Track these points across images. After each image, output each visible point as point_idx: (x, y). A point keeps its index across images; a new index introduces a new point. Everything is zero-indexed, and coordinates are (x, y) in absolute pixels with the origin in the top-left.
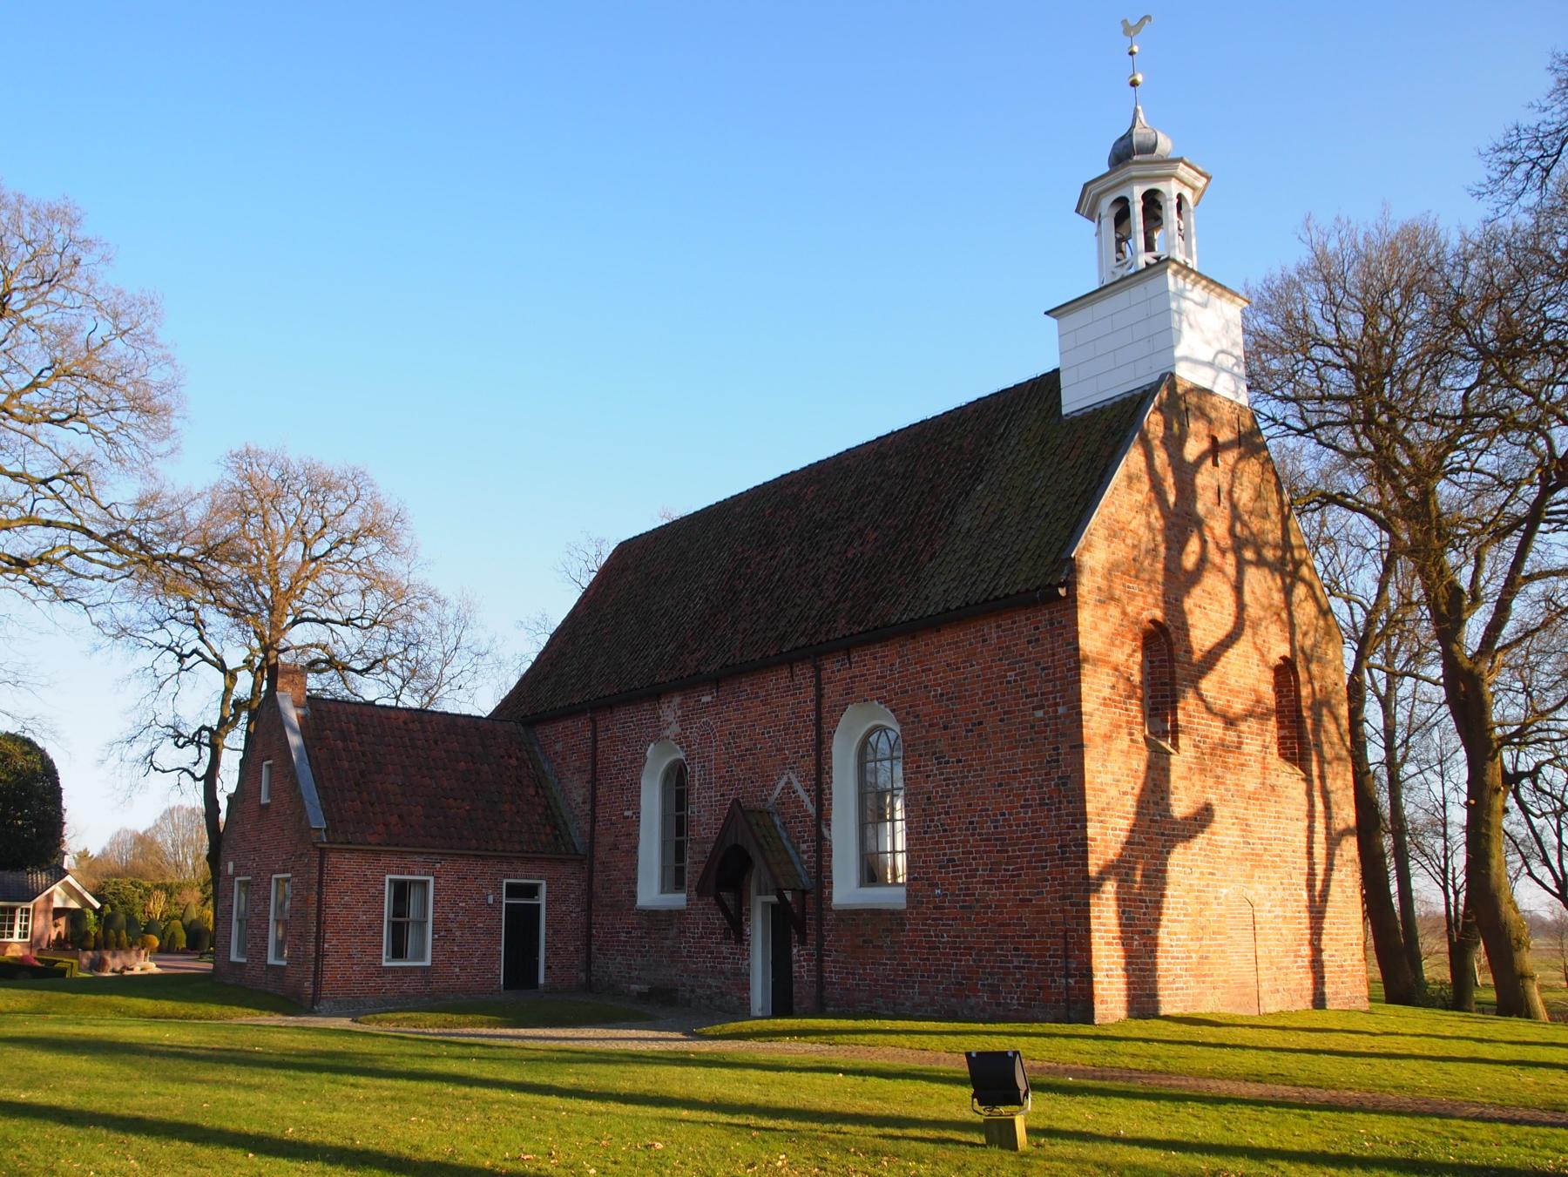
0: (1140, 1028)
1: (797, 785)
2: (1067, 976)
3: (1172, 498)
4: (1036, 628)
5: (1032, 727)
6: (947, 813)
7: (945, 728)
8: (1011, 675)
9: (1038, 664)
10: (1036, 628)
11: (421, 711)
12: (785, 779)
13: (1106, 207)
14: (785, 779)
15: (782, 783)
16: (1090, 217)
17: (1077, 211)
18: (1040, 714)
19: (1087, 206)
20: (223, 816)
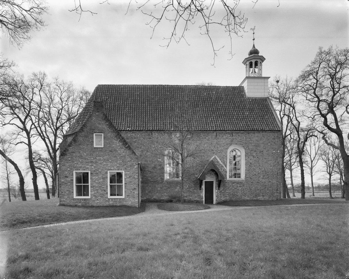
0: (314, 197)
1: (217, 158)
2: (277, 193)
3: (55, 128)
4: (274, 137)
5: (273, 153)
6: (255, 166)
7: (255, 151)
8: (269, 144)
9: (274, 143)
10: (274, 137)
11: (335, 123)
12: (214, 157)
13: (248, 63)
14: (214, 157)
15: (213, 157)
16: (245, 64)
17: (243, 63)
18: (274, 151)
19: (244, 62)
20: (53, 147)
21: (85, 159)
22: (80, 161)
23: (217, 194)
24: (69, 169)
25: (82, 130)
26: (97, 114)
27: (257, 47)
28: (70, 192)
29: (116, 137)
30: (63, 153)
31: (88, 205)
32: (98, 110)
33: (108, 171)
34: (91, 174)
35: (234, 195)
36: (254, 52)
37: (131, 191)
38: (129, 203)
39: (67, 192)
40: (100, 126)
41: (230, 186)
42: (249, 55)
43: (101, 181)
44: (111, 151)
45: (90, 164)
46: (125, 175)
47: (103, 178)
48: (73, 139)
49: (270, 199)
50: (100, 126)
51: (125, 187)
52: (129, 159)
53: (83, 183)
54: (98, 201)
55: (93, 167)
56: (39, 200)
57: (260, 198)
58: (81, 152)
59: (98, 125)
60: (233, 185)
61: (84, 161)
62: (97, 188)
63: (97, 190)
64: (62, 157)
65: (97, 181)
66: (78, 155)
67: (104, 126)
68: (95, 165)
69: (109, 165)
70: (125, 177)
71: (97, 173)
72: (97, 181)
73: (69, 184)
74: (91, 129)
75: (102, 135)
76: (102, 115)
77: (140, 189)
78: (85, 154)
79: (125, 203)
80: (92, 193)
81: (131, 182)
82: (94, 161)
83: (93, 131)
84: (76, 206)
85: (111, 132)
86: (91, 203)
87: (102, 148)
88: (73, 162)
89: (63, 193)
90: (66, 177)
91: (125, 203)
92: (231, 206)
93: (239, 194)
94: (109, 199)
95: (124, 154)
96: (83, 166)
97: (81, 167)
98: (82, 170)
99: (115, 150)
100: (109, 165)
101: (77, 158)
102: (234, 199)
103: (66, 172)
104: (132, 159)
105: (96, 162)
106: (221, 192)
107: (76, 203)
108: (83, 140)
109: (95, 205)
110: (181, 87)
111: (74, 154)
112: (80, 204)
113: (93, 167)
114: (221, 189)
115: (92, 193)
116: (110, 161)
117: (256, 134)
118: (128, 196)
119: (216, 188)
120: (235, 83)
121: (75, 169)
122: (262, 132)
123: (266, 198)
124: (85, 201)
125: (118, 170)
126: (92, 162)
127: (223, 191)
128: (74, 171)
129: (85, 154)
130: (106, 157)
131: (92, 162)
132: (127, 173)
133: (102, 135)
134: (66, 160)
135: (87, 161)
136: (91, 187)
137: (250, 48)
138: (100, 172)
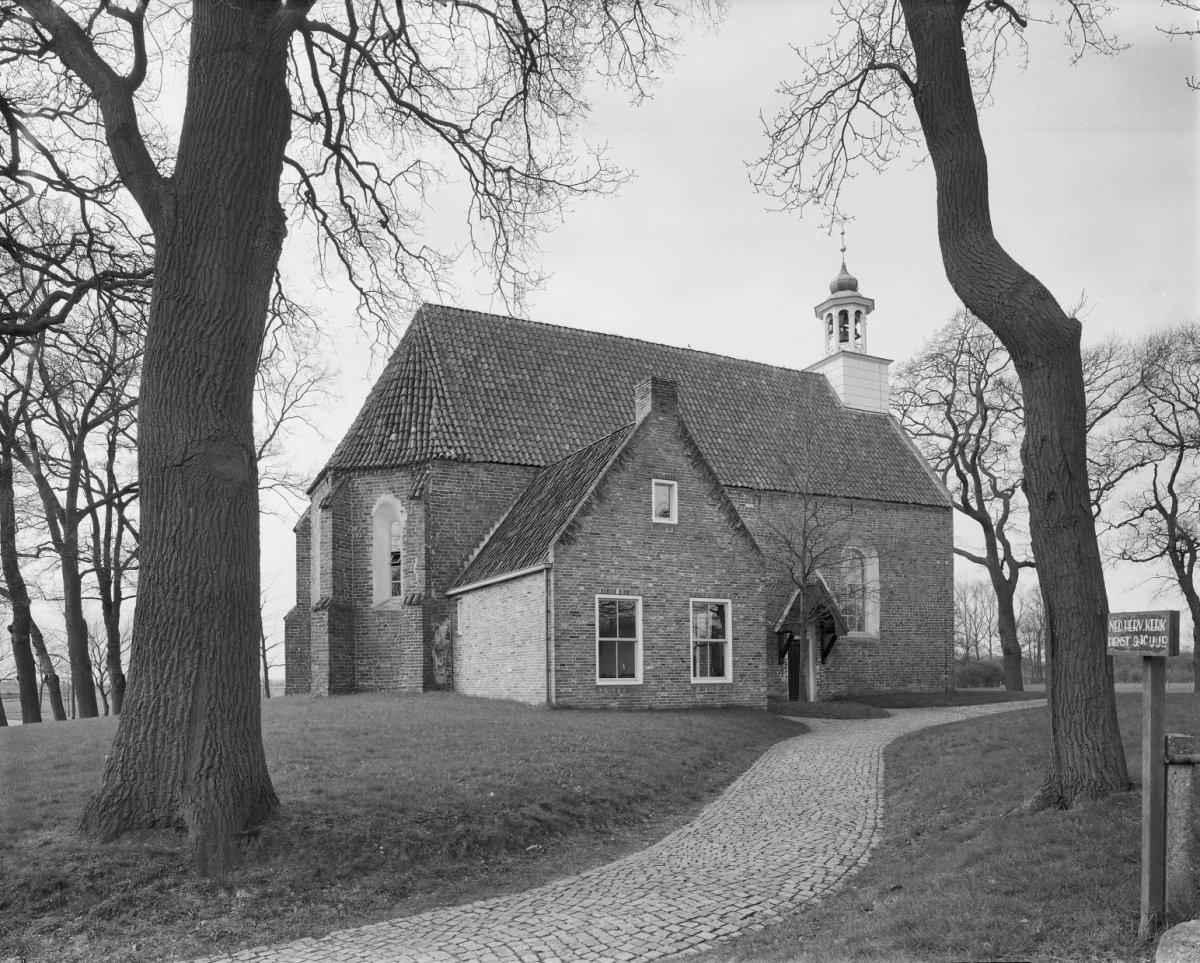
18: (938, 562)
19: (819, 312)
21: (630, 558)
22: (616, 563)
23: (818, 677)
24: (582, 588)
25: (621, 464)
26: (661, 418)
27: (853, 272)
28: (586, 663)
29: (711, 495)
30: (567, 535)
31: (637, 705)
32: (665, 408)
33: (692, 600)
34: (646, 606)
35: (857, 680)
36: (847, 285)
37: (751, 661)
38: (744, 699)
39: (577, 665)
40: (670, 458)
41: (849, 654)
42: (833, 292)
43: (672, 629)
44: (698, 538)
45: (643, 576)
46: (735, 611)
47: (678, 621)
48: (596, 493)
49: (933, 691)
50: (670, 458)
51: (735, 649)
52: (743, 566)
53: (620, 637)
54: (663, 694)
55: (651, 585)
56: (95, 718)
57: (913, 687)
58: (618, 535)
59: (664, 454)
60: (855, 650)
61: (627, 563)
62: (662, 652)
63: (662, 658)
64: (562, 547)
65: (661, 631)
66: (611, 544)
67: (680, 460)
68: (655, 579)
69: (693, 581)
70: (735, 619)
71: (662, 606)
72: (661, 631)
73: (584, 637)
74: (645, 465)
75: (671, 486)
76: (675, 424)
77: (76, 703)
78: (628, 542)
79: (734, 699)
80: (648, 668)
81: (748, 634)
82: (653, 565)
83: (649, 471)
84: (605, 709)
85: (699, 479)
86: (647, 700)
87: (673, 525)
88: (595, 565)
89: (566, 668)
90: (575, 614)
91: (734, 699)
92: (922, 706)
93: (869, 675)
94: (694, 686)
95: (731, 549)
96: (623, 580)
97: (617, 584)
98: (620, 594)
99: (710, 536)
100: (693, 581)
101: (608, 554)
102: (856, 691)
103: (576, 600)
104: (751, 565)
105: (660, 571)
106: (827, 671)
107: (605, 702)
108: (624, 496)
109: (657, 704)
110: (562, 330)
111: (598, 542)
112: (615, 704)
113: (651, 585)
114: (830, 660)
115: (648, 668)
116: (696, 567)
117: (902, 514)
118: (742, 676)
119: (816, 659)
120: (796, 360)
121: (599, 589)
122: (914, 509)
123: (925, 687)
124: (629, 695)
125: (717, 597)
126: (647, 569)
127: (833, 669)
128: (598, 596)
129: (628, 542)
130: (686, 554)
131: (647, 569)
132: (739, 605)
133: (671, 486)
134: (575, 558)
135: (635, 565)
136: (646, 648)
137: (834, 275)
138: (670, 602)
